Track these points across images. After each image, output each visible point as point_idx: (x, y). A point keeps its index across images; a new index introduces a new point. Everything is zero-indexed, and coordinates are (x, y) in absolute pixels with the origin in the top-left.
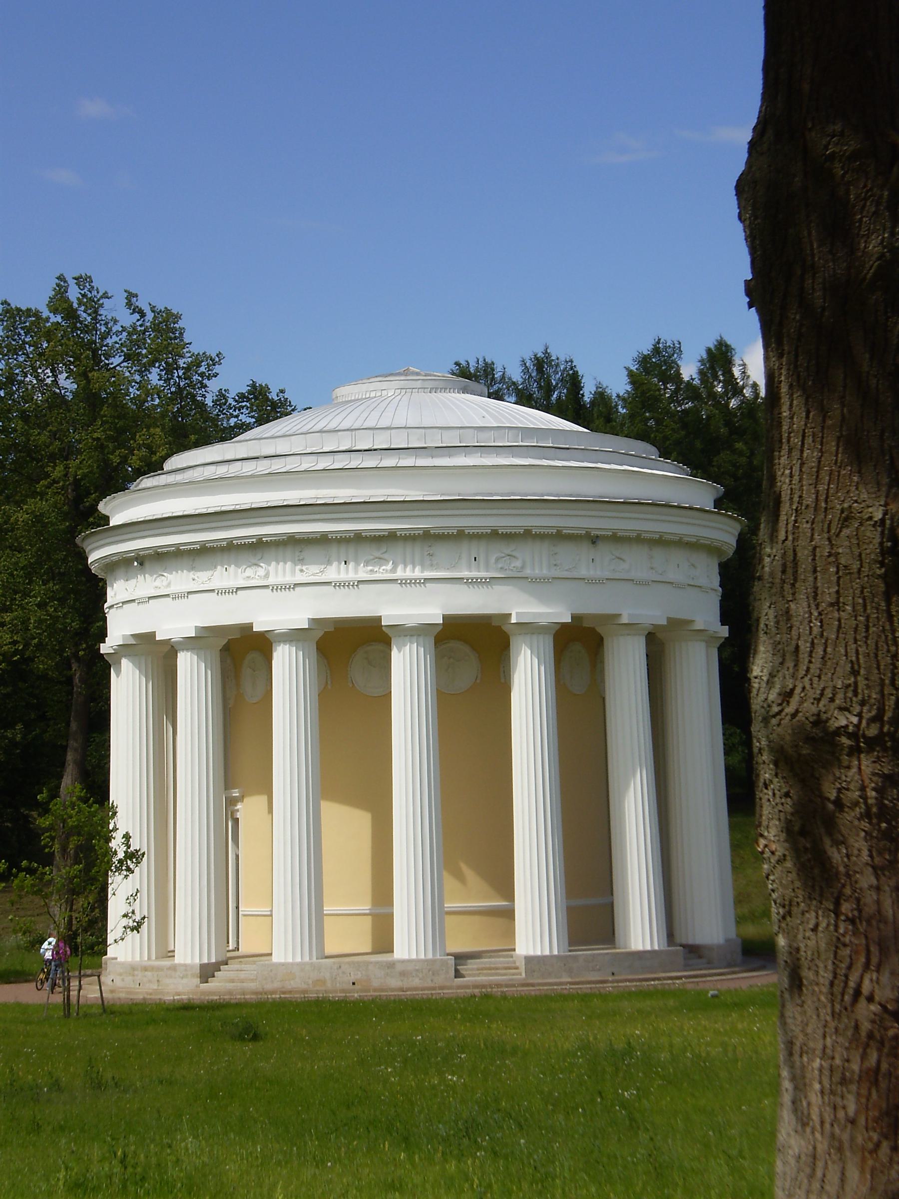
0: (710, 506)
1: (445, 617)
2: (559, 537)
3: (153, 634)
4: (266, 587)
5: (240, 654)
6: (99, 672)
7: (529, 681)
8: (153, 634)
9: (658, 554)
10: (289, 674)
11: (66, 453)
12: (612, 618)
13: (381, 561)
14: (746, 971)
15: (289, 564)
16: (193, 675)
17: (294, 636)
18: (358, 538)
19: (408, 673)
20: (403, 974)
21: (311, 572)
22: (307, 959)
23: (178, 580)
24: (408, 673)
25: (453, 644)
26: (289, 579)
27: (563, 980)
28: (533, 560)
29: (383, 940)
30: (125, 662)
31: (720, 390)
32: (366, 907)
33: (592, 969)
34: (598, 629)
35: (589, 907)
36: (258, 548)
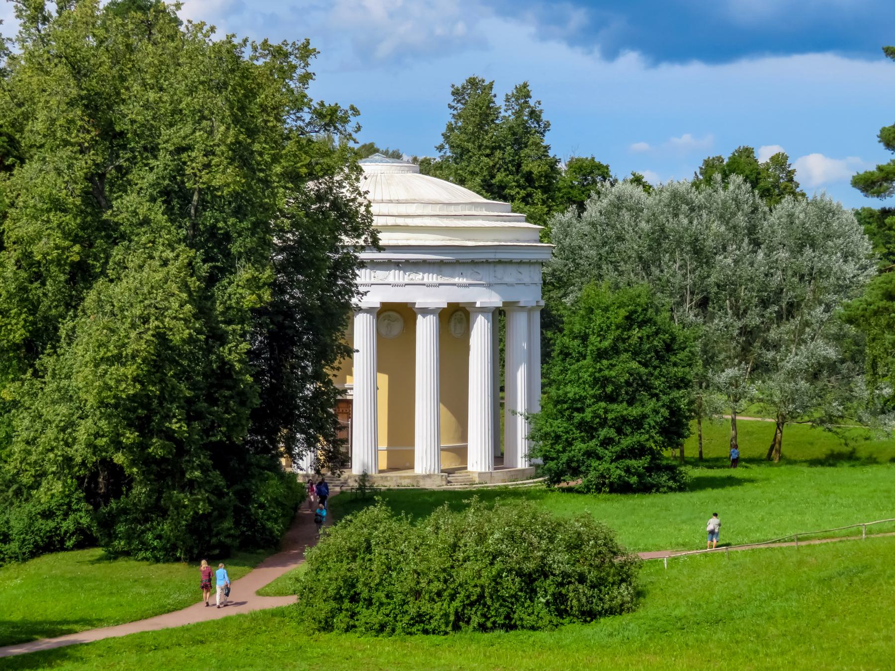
1: (448, 304)
13: (453, 276)
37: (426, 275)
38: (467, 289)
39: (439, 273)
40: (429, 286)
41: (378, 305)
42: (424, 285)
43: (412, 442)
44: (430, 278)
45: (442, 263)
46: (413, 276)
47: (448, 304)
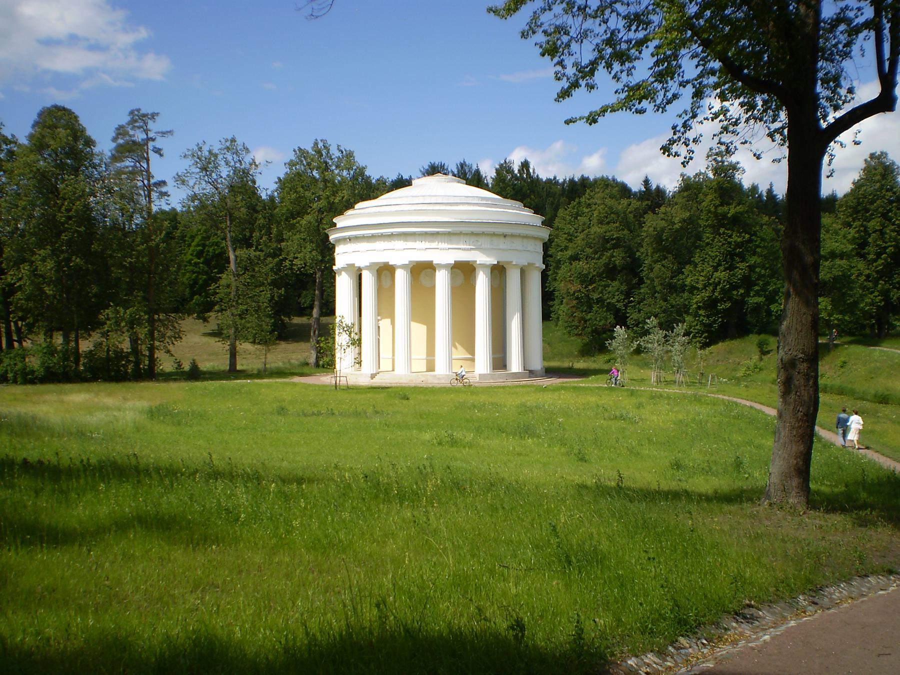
0: (539, 224)
2: (494, 235)
5: (385, 271)
6: (330, 277)
7: (482, 283)
9: (525, 241)
10: (401, 279)
11: (319, 199)
12: (510, 263)
13: (433, 241)
16: (368, 280)
17: (403, 267)
18: (426, 233)
19: (442, 280)
20: (439, 379)
21: (410, 244)
24: (442, 280)
25: (458, 271)
27: (491, 382)
28: (485, 242)
29: (431, 367)
30: (343, 273)
31: (783, 67)
32: (425, 357)
33: (499, 378)
35: (500, 361)
36: (391, 236)
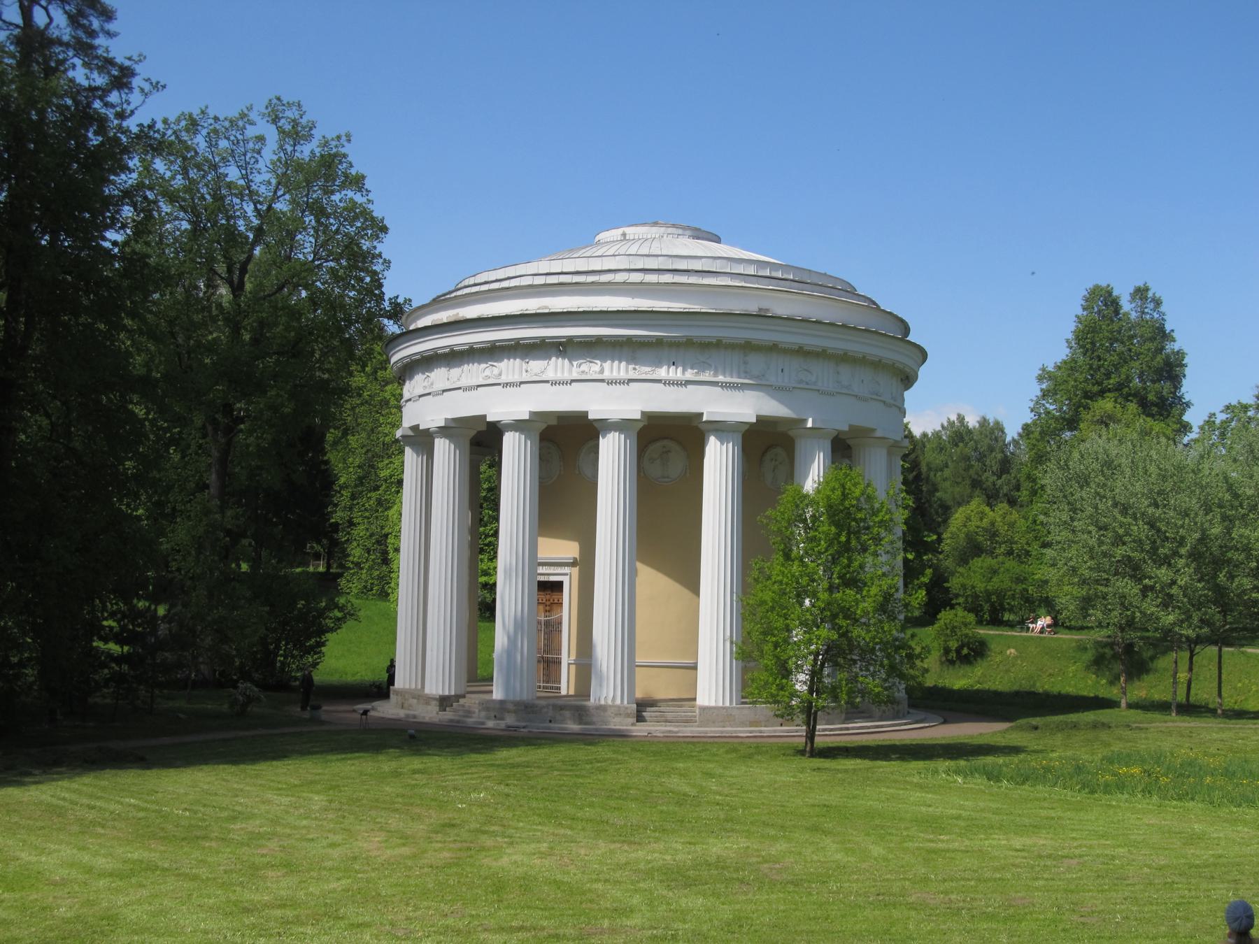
1: (643, 413)
2: (802, 352)
3: (485, 416)
4: (602, 381)
8: (485, 416)
13: (658, 364)
14: (917, 722)
15: (624, 364)
22: (727, 704)
23: (509, 368)
26: (623, 375)
34: (791, 433)
37: (607, 365)
38: (473, 393)
39: (632, 360)
40: (611, 382)
41: (638, 416)
42: (602, 381)
43: (394, 642)
44: (615, 369)
45: (658, 343)
46: (585, 367)
47: (643, 413)
